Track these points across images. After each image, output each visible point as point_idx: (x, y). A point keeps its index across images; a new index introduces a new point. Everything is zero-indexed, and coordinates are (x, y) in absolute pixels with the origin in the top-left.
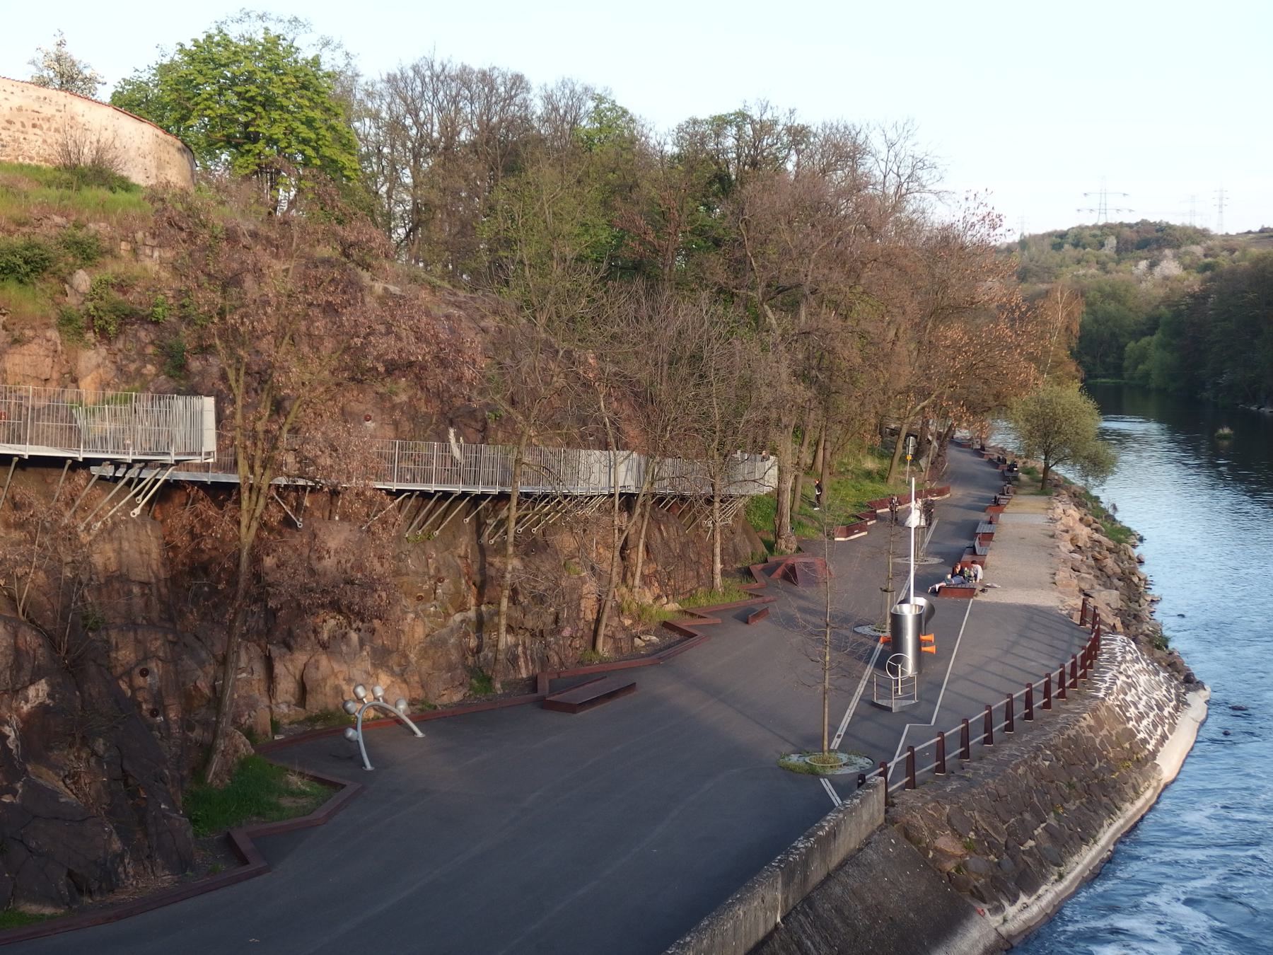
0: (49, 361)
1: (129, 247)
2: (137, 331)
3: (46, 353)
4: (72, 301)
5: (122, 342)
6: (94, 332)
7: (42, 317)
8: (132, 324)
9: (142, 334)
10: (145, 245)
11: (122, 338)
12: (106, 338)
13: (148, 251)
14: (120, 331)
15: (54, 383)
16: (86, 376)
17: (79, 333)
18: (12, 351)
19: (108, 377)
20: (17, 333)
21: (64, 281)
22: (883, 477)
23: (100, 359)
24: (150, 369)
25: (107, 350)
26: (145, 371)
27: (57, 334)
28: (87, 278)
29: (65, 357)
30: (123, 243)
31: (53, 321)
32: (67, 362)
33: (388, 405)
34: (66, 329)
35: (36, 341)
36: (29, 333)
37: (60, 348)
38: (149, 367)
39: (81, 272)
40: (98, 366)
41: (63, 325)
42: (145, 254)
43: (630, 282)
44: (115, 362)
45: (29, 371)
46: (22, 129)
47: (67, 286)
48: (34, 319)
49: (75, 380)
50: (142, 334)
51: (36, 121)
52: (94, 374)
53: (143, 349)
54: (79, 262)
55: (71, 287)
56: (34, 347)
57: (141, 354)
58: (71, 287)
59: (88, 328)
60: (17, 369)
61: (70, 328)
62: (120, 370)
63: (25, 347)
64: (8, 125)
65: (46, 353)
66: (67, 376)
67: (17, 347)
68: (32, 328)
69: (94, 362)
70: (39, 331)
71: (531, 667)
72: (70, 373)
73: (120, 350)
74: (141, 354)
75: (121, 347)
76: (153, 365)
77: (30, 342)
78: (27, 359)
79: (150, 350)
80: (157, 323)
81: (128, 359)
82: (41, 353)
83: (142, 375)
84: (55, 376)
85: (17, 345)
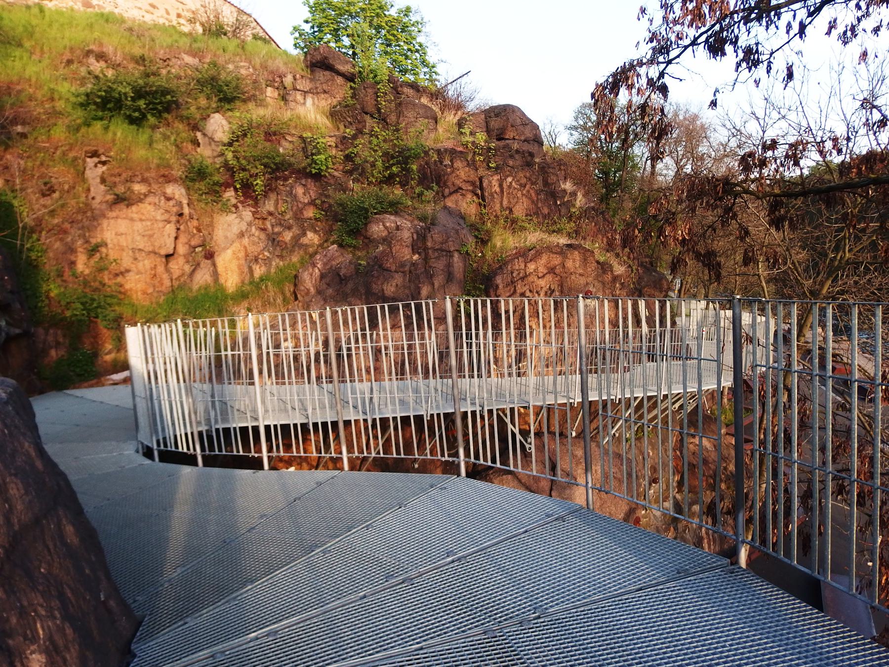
0: (170, 229)
1: (276, 94)
2: (292, 187)
3: (166, 216)
4: (205, 153)
5: (272, 202)
6: (236, 190)
7: (158, 166)
8: (286, 179)
9: (300, 190)
10: (295, 89)
11: (273, 196)
12: (251, 198)
13: (299, 97)
14: (269, 189)
15: (181, 261)
16: (227, 248)
17: (215, 191)
18: (114, 214)
19: (254, 250)
20: (120, 189)
21: (195, 128)
22: (450, 277)
23: (244, 227)
24: (312, 238)
25: (254, 213)
26: (304, 240)
27: (183, 191)
28: (224, 122)
29: (195, 223)
30: (269, 89)
31: (178, 172)
32: (199, 230)
33: (609, 277)
34: (197, 185)
35: (150, 199)
36: (138, 188)
37: (186, 210)
38: (310, 235)
39: (217, 116)
40: (242, 235)
41: (193, 180)
42: (295, 101)
43: (131, 290)
44: (264, 230)
45: (141, 243)
46: (166, 16)
47: (199, 135)
48: (148, 169)
49: (210, 256)
50: (300, 190)
51: (180, 11)
52: (237, 245)
53: (301, 211)
54: (214, 105)
55: (205, 135)
56: (146, 208)
57: (298, 217)
58: (205, 135)
59: (227, 185)
60: (123, 241)
61: (202, 186)
62: (273, 240)
63: (134, 208)
64: (151, 9)
65: (166, 216)
66: (198, 249)
67: (122, 211)
68: (144, 180)
69: (235, 230)
70: (155, 186)
71: (712, 547)
72: (203, 245)
73: (270, 214)
74: (298, 217)
75: (272, 209)
76: (315, 232)
77: (140, 201)
78: (138, 226)
79: (310, 213)
80: (317, 177)
81: (281, 225)
82: (159, 218)
83: (301, 246)
84: (182, 249)
85: (122, 206)
